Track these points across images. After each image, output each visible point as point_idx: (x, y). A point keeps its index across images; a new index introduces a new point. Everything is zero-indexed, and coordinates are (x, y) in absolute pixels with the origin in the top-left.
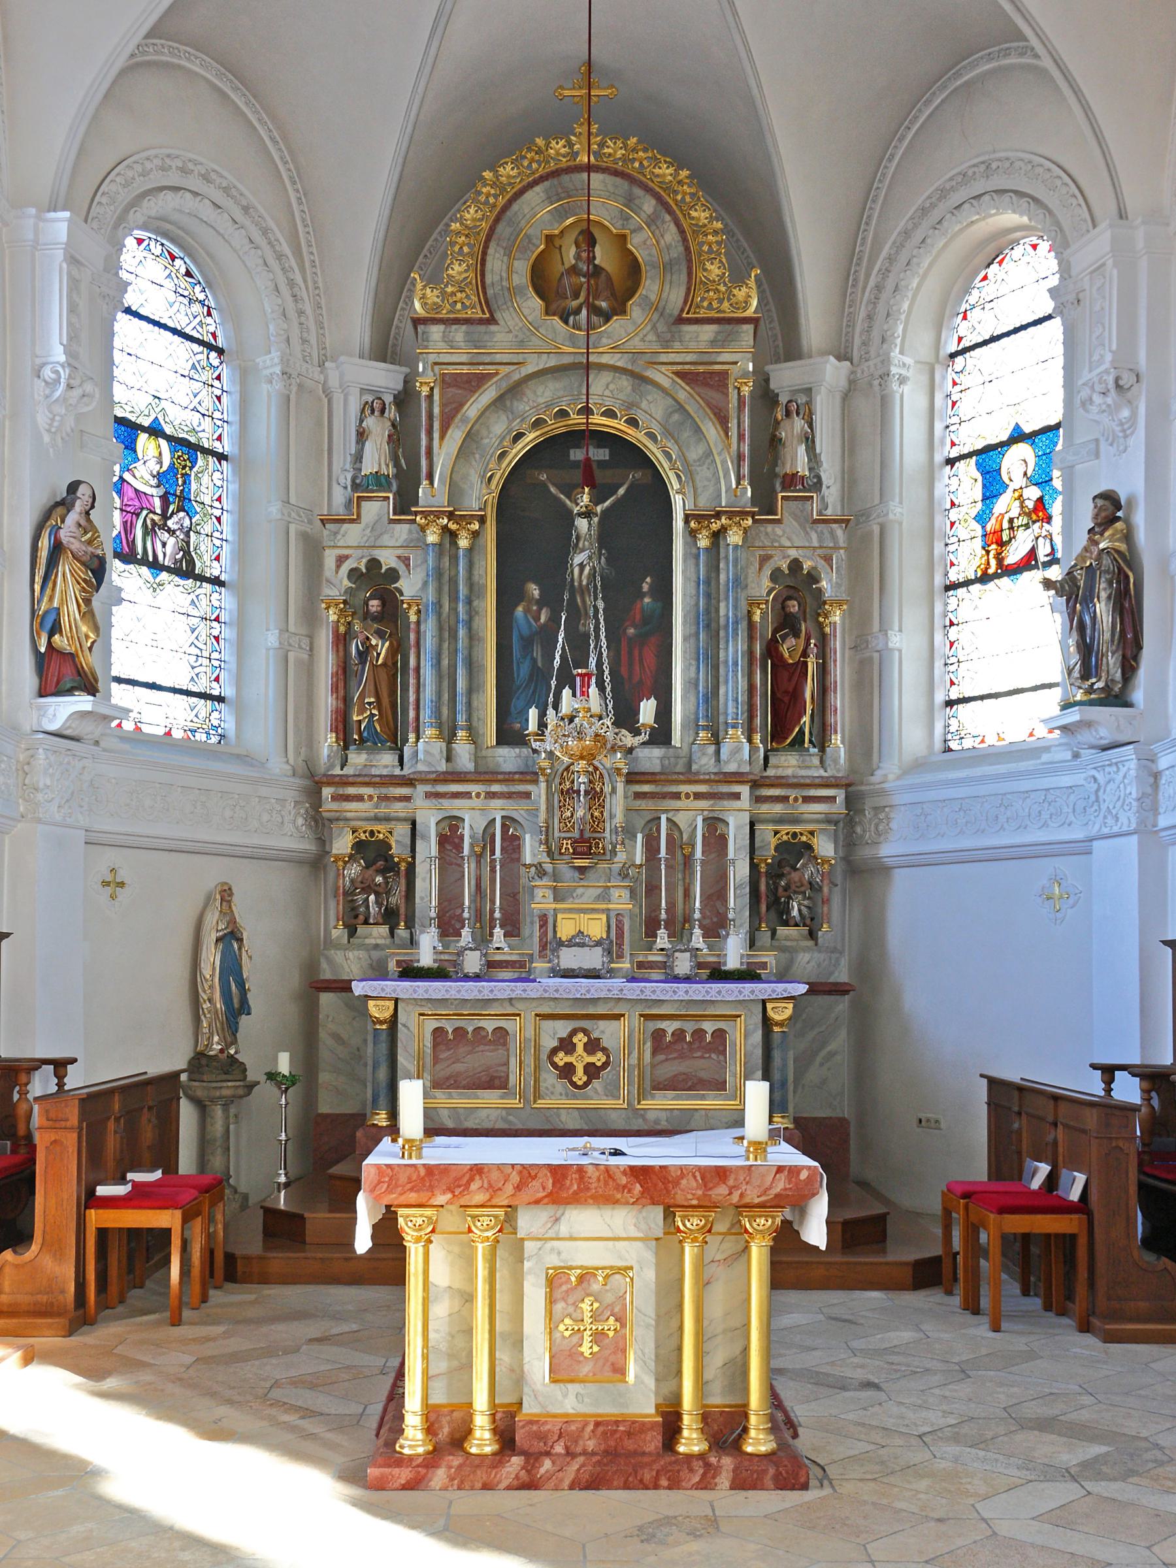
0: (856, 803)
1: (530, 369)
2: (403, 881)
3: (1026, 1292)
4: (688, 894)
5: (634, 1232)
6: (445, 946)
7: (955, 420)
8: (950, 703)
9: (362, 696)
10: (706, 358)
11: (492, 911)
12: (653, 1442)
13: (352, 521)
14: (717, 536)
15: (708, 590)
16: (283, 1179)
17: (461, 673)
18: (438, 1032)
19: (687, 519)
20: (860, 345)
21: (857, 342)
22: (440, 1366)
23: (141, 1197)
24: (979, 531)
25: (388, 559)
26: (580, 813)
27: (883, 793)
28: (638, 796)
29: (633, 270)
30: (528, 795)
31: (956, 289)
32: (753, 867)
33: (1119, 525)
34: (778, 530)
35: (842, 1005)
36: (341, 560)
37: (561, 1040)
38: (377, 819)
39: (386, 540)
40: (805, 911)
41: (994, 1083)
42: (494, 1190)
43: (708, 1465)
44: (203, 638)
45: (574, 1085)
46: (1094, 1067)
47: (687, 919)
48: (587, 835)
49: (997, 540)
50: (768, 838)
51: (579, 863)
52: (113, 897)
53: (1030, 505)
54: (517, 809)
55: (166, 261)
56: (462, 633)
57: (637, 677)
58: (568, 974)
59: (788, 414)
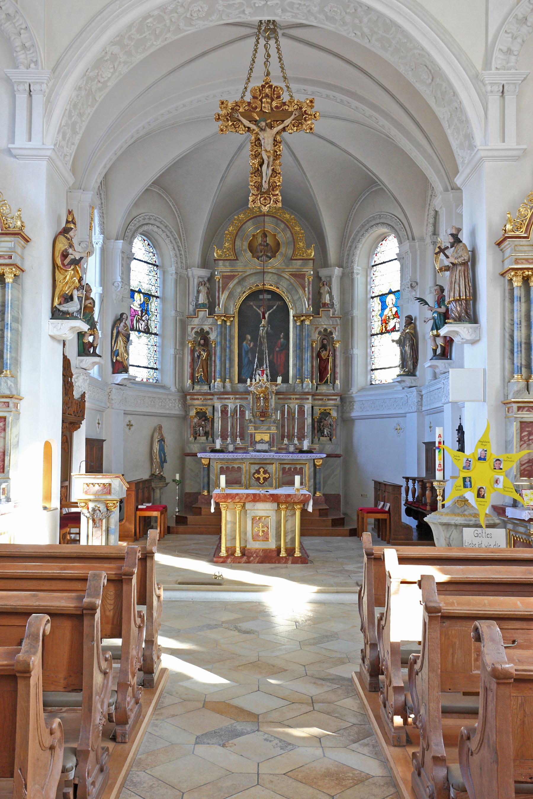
0: (345, 400)
1: (248, 273)
2: (210, 423)
3: (379, 537)
4: (294, 428)
5: (271, 509)
6: (223, 443)
7: (373, 285)
8: (372, 370)
9: (198, 369)
10: (299, 270)
11: (237, 433)
12: (275, 554)
13: (196, 317)
14: (302, 321)
15: (300, 337)
16: (177, 510)
17: (227, 362)
18: (222, 468)
19: (294, 317)
20: (345, 264)
21: (345, 262)
22: (229, 538)
23: (148, 509)
24: (380, 319)
25: (206, 328)
26: (262, 404)
27: (352, 397)
28: (279, 399)
29: (278, 245)
30: (247, 398)
31: (373, 248)
32: (313, 419)
33: (412, 325)
34: (320, 320)
35: (339, 461)
36: (193, 329)
37: (256, 470)
38: (203, 405)
39: (206, 323)
40: (328, 432)
41: (376, 482)
42: (241, 499)
43: (286, 559)
44: (152, 351)
45: (260, 483)
46: (404, 478)
47: (293, 435)
48: (264, 411)
49: (385, 322)
50: (318, 411)
51: (261, 419)
52: (130, 429)
53: (394, 313)
54: (244, 403)
55: (142, 242)
56: (227, 350)
57: (278, 370)
58: (259, 451)
59: (323, 285)
